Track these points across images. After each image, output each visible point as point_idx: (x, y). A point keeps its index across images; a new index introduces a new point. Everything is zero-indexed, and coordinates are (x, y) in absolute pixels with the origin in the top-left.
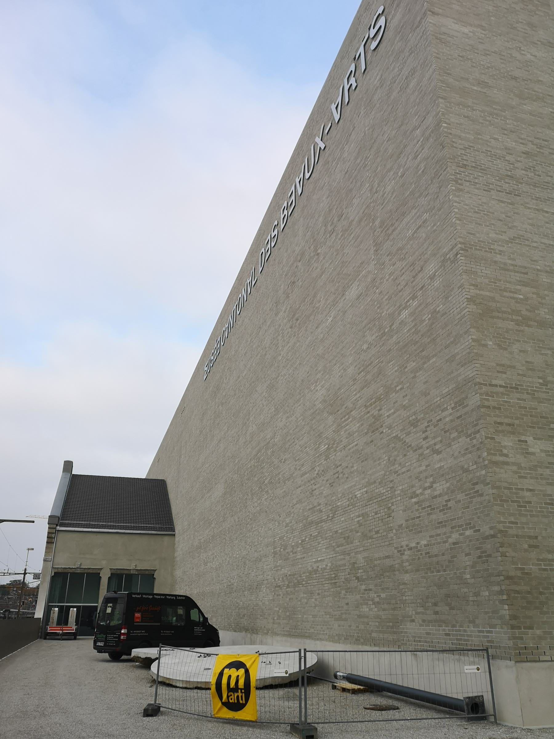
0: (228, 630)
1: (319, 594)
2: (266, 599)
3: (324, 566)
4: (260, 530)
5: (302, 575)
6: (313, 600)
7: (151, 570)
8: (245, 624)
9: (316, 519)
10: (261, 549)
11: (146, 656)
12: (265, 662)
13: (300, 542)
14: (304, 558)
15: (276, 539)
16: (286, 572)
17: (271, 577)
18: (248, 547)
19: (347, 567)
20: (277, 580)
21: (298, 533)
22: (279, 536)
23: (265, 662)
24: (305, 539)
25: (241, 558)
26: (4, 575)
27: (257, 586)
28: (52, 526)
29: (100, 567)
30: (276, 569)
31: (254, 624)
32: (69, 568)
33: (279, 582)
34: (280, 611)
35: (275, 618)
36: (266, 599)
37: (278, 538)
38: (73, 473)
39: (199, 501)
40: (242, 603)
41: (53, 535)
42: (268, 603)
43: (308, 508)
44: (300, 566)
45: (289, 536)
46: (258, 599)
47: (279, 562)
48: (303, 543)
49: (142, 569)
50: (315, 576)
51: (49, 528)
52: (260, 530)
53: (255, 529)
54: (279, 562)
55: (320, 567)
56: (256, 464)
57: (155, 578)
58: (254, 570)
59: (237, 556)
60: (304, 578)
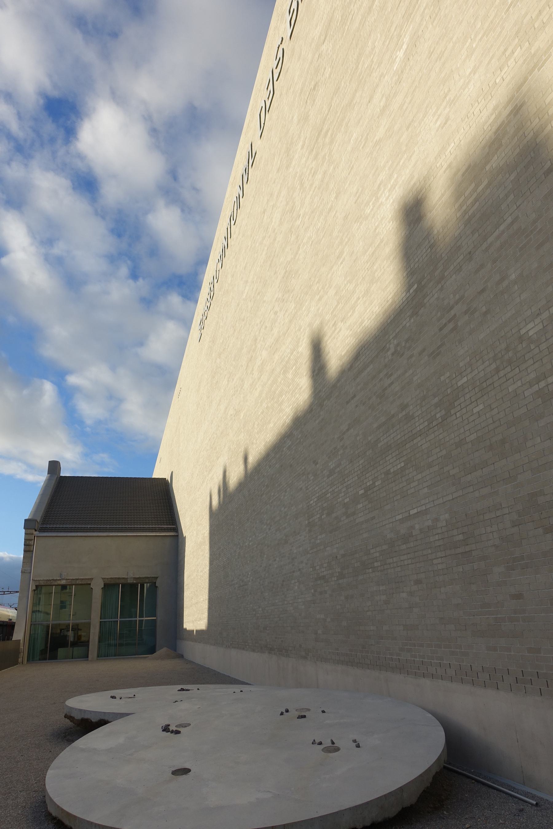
0: (243, 649)
1: (418, 582)
2: (300, 600)
3: (430, 523)
4: (282, 498)
5: (372, 551)
6: (404, 595)
7: (152, 577)
8: (268, 641)
9: (399, 437)
10: (286, 524)
11: (83, 716)
12: (320, 743)
13: (361, 492)
14: (373, 518)
15: (312, 502)
16: (335, 550)
17: (306, 564)
18: (265, 527)
19: (506, 511)
20: (318, 568)
21: (356, 478)
22: (317, 495)
23: (320, 743)
24: (374, 483)
25: (256, 545)
26: (4, 594)
27: (283, 581)
28: (29, 531)
29: (90, 577)
30: (315, 550)
31: (282, 641)
32: (53, 580)
33: (323, 570)
34: (329, 620)
35: (320, 632)
36: (300, 600)
37: (316, 499)
38: (61, 475)
39: (200, 488)
40: (261, 609)
41: (32, 543)
42: (303, 607)
43: (375, 426)
44: (365, 535)
45: (336, 490)
46: (286, 602)
47: (319, 537)
48: (369, 492)
49: (141, 576)
50: (404, 547)
51: (25, 534)
52: (282, 498)
53: (274, 498)
54: (319, 537)
55: (417, 527)
56: (270, 405)
57: (157, 587)
58: (277, 559)
59: (251, 544)
60: (378, 554)
